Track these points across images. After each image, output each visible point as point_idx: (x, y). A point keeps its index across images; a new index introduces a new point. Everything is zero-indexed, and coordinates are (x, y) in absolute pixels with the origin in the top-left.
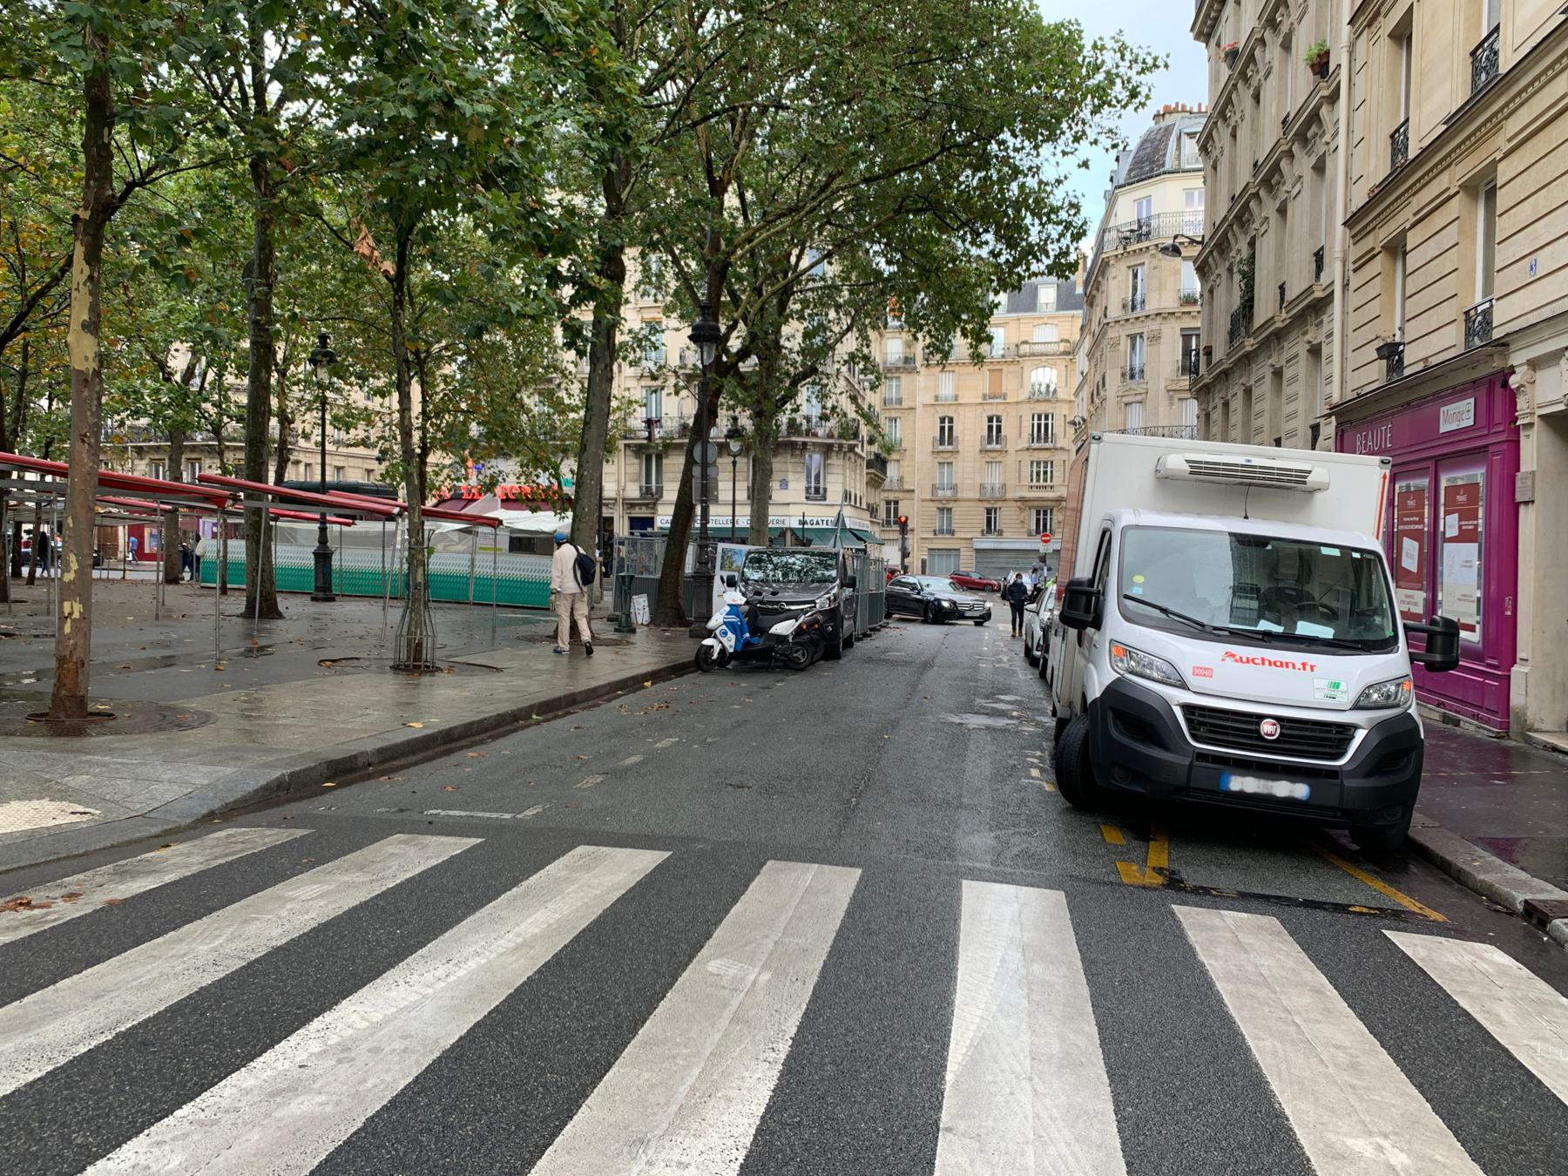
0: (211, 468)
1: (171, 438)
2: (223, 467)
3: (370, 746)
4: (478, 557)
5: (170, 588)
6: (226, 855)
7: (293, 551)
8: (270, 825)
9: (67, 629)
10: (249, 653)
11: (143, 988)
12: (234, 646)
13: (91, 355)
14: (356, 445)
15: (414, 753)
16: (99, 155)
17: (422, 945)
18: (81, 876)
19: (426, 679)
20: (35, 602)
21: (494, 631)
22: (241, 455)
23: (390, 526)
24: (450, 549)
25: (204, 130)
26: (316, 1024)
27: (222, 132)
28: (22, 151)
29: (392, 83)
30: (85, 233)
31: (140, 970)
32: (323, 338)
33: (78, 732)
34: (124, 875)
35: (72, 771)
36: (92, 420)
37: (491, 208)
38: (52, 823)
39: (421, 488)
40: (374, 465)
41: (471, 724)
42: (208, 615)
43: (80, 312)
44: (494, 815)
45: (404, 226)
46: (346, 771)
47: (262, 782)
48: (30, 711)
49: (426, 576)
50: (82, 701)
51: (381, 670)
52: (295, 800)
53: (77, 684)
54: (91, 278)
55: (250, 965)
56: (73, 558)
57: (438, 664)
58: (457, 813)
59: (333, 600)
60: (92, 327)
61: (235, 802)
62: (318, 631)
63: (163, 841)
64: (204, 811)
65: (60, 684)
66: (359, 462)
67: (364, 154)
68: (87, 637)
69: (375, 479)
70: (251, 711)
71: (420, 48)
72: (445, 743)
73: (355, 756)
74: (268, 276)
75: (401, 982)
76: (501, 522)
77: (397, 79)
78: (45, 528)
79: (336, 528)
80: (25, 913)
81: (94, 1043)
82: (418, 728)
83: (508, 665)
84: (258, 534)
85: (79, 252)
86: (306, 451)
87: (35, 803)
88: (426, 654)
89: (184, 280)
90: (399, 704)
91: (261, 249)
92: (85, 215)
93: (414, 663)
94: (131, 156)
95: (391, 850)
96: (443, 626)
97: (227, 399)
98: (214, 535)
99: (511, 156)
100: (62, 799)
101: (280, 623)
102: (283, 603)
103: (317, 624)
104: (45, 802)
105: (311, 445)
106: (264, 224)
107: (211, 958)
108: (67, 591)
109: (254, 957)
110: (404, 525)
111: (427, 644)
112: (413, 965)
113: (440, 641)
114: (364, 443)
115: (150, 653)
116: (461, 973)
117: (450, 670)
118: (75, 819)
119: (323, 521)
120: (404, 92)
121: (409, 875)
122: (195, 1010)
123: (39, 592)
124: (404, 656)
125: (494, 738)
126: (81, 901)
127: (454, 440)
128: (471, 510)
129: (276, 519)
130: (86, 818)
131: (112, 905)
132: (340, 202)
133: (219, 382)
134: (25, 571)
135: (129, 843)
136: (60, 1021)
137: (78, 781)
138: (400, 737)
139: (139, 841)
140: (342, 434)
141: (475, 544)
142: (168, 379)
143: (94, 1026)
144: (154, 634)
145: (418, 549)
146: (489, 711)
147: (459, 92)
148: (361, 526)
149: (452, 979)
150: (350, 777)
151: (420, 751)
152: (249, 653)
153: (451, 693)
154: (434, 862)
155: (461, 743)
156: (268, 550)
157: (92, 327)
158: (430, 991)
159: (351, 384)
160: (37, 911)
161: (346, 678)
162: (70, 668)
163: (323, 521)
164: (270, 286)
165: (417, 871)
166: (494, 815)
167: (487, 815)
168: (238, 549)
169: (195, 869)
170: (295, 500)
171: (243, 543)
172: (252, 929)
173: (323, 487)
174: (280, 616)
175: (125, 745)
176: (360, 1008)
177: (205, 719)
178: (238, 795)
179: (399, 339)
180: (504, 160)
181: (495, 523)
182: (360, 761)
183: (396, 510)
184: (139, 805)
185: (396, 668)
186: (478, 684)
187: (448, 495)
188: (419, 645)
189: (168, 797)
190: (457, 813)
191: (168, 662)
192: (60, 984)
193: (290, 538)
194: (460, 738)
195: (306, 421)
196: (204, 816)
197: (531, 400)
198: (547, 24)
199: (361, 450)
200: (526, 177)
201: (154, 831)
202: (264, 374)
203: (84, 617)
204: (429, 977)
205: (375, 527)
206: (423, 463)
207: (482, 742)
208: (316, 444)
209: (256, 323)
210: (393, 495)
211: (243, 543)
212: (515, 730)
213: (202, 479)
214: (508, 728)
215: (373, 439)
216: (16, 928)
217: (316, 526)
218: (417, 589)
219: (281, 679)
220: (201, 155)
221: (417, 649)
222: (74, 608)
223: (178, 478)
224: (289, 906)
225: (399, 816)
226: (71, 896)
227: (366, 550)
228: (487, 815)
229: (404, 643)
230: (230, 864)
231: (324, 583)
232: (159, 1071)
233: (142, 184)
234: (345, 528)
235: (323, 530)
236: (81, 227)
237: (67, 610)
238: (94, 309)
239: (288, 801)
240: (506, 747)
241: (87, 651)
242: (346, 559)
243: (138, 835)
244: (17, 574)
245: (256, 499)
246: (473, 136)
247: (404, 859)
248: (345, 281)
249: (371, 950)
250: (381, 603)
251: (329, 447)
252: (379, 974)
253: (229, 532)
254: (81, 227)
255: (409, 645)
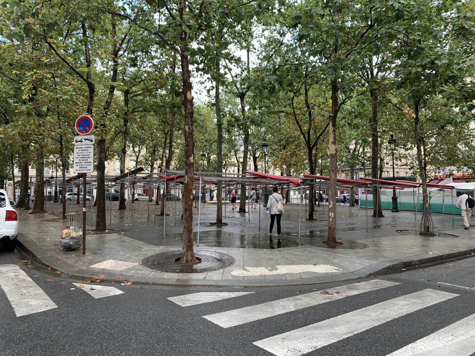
0: (362, 175)
1: (351, 167)
2: (365, 174)
3: (416, 259)
4: (445, 198)
5: (352, 207)
6: (376, 287)
7: (386, 196)
8: (388, 280)
9: (331, 220)
10: (375, 227)
11: (359, 323)
12: (371, 225)
13: (334, 150)
14: (403, 166)
15: (430, 262)
16: (335, 98)
17: (442, 328)
18: (339, 287)
19: (431, 238)
20: (320, 211)
21: (453, 223)
22: (371, 170)
23: (416, 189)
24: (436, 198)
25: (359, 86)
26: (410, 346)
27: (363, 85)
28: (315, 101)
29: (414, 62)
30: (332, 119)
31: (357, 317)
32: (392, 136)
33: (334, 247)
34: (350, 289)
35: (334, 258)
36: (335, 166)
37: (449, 91)
38: (331, 272)
39: (424, 175)
40: (408, 171)
41: (449, 254)
42: (363, 216)
43: (331, 140)
44: (462, 287)
45: (417, 101)
46: (409, 266)
47: (384, 267)
48: (323, 241)
49: (429, 205)
50: (335, 239)
51: (416, 234)
52: (394, 273)
53: (333, 235)
54: (334, 130)
55: (388, 322)
56: (331, 202)
57: (435, 233)
58: (449, 284)
59: (398, 212)
60: (334, 143)
61: (377, 271)
62: (395, 221)
63: (359, 280)
64: (369, 273)
65: (329, 234)
66: (403, 170)
67: (404, 83)
68: (335, 222)
69: (409, 175)
70: (376, 245)
71: (422, 49)
72: (441, 260)
73: (411, 261)
74: (376, 121)
75: (436, 338)
76: (454, 187)
77: (415, 60)
78: (321, 192)
79: (398, 190)
80: (327, 295)
81: (348, 336)
82: (431, 254)
83: (460, 235)
84: (376, 193)
85: (331, 124)
86: (387, 168)
87: (326, 266)
88: (431, 230)
89: (356, 127)
90: (423, 246)
91: (374, 114)
92: (332, 115)
93: (427, 233)
94: (341, 96)
95: (427, 293)
96: (435, 220)
97: (366, 156)
98: (363, 193)
99: (453, 73)
100: (332, 265)
101: (383, 218)
102: (384, 212)
103: (394, 219)
104: (329, 265)
105: (389, 166)
106: (375, 108)
107: (376, 317)
108: (330, 210)
109: (388, 320)
110: (421, 189)
111: (431, 227)
112: (440, 334)
113: (435, 226)
114: (406, 165)
115: (349, 226)
116: (457, 340)
117: (439, 235)
118: (336, 271)
119: (394, 188)
120: (418, 64)
121: (435, 303)
122: (373, 333)
123: (320, 209)
124: (423, 230)
125: (458, 260)
126: (340, 294)
127: (434, 161)
128: (441, 183)
129: (381, 188)
130: (338, 271)
131: (348, 297)
132: (396, 96)
133: (363, 152)
134: (317, 203)
135: (350, 280)
136: (339, 327)
137: (336, 261)
138: (425, 257)
139: (352, 279)
140: (399, 162)
141: (444, 194)
142: (350, 152)
143: (348, 331)
144: (349, 221)
145: (426, 196)
146: (456, 250)
147: (436, 59)
148: (406, 190)
149: (454, 341)
150: (410, 267)
151: (432, 261)
152: (375, 227)
153: (442, 243)
154: (443, 300)
155: (446, 260)
156: (379, 197)
157: (334, 143)
158: (447, 344)
159: (401, 148)
160: (330, 295)
161: (405, 236)
162: (332, 230)
163: (394, 188)
164: (377, 124)
165: (437, 302)
166: (462, 287)
167: (460, 286)
168: (370, 197)
169: (368, 290)
170: (387, 182)
171: (372, 195)
172: (387, 311)
173: (394, 179)
174: (383, 216)
175: (346, 252)
176: (423, 344)
177: (365, 246)
178: (378, 270)
179: (417, 134)
180: (451, 74)
181: (452, 188)
182: (413, 263)
183: (418, 185)
184: (351, 270)
185: (421, 234)
186: (450, 241)
187: (433, 178)
188: (428, 227)
189: (359, 268)
190: (449, 284)
191: (352, 229)
192: (338, 317)
193: (385, 193)
194: (446, 259)
195: (387, 159)
196: (369, 275)
197: (461, 146)
198: (467, 29)
199: (405, 167)
200: (459, 78)
201: (356, 277)
202: (376, 148)
203: (335, 217)
204: (446, 339)
205: (411, 189)
206: (425, 169)
207: (454, 261)
208: (391, 165)
209: (373, 134)
210: (415, 180)
211: (372, 195)
212: (466, 258)
213: (361, 178)
214: (463, 257)
215: (409, 164)
216: (326, 299)
217: (392, 190)
218: (425, 209)
219: (385, 236)
220: (358, 93)
221: (428, 228)
222: (332, 214)
223: (353, 178)
224: (397, 306)
225: (428, 283)
226: (338, 293)
227: (407, 196)
228: (460, 286)
229: (423, 226)
230: (378, 290)
231: (395, 207)
232: (366, 348)
233: (343, 104)
234: (401, 190)
235: (394, 191)
236: (331, 118)
237: (330, 215)
238: (335, 138)
239: (392, 273)
240: (464, 263)
241: (335, 226)
242: (401, 199)
243: (352, 278)
244: (315, 204)
245: (376, 182)
246: (441, 70)
247: (432, 298)
248: (398, 119)
249: (425, 326)
250: (414, 213)
251: (395, 166)
252: (429, 334)
253: (369, 192)
254: (331, 118)
255: (425, 226)
